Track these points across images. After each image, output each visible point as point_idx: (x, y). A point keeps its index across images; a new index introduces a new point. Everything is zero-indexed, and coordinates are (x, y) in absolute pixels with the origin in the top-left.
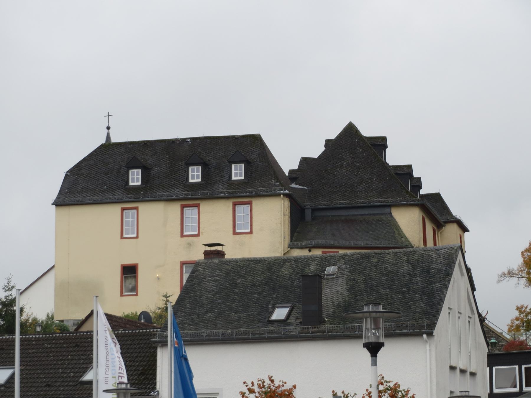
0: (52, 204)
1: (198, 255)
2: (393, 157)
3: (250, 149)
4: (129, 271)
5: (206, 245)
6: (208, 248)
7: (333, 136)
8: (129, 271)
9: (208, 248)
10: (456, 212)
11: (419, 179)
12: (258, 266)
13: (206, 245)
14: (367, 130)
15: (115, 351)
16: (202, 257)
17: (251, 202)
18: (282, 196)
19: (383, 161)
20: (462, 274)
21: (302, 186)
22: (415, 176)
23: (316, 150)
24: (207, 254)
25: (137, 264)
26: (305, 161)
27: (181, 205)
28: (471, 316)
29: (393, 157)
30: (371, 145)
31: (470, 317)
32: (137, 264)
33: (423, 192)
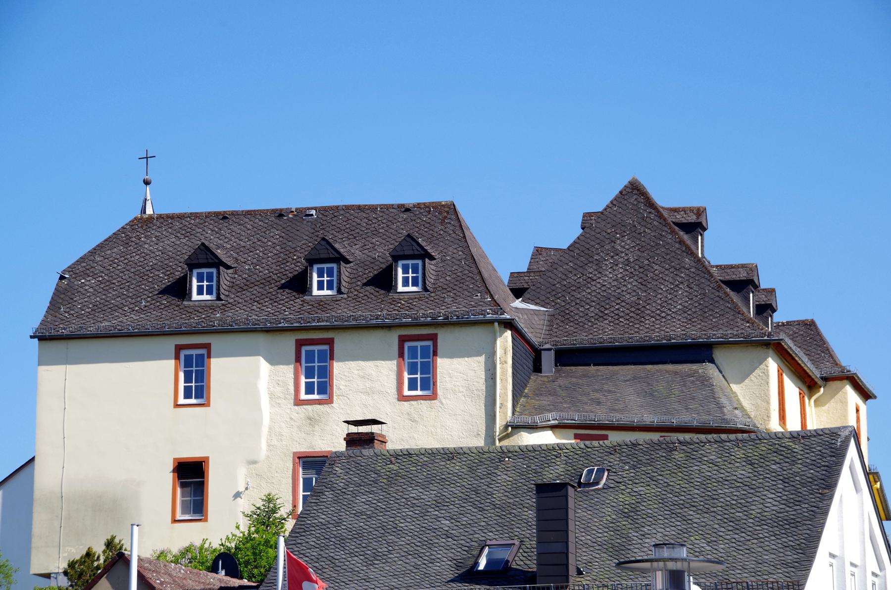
0: (31, 337)
1: (332, 440)
2: (718, 249)
3: (425, 235)
4: (191, 474)
5: (348, 422)
6: (354, 429)
7: (599, 206)
8: (191, 474)
9: (354, 429)
10: (848, 359)
11: (772, 291)
12: (456, 467)
13: (348, 422)
14: (666, 197)
15: (237, 585)
16: (341, 446)
17: (436, 335)
18: (496, 324)
19: (697, 256)
20: (857, 489)
21: (537, 304)
22: (763, 285)
23: (564, 234)
24: (352, 441)
25: (208, 458)
26: (588, 220)
27: (297, 341)
28: (877, 571)
29: (718, 249)
30: (674, 223)
31: (874, 574)
32: (208, 458)
33: (779, 317)
